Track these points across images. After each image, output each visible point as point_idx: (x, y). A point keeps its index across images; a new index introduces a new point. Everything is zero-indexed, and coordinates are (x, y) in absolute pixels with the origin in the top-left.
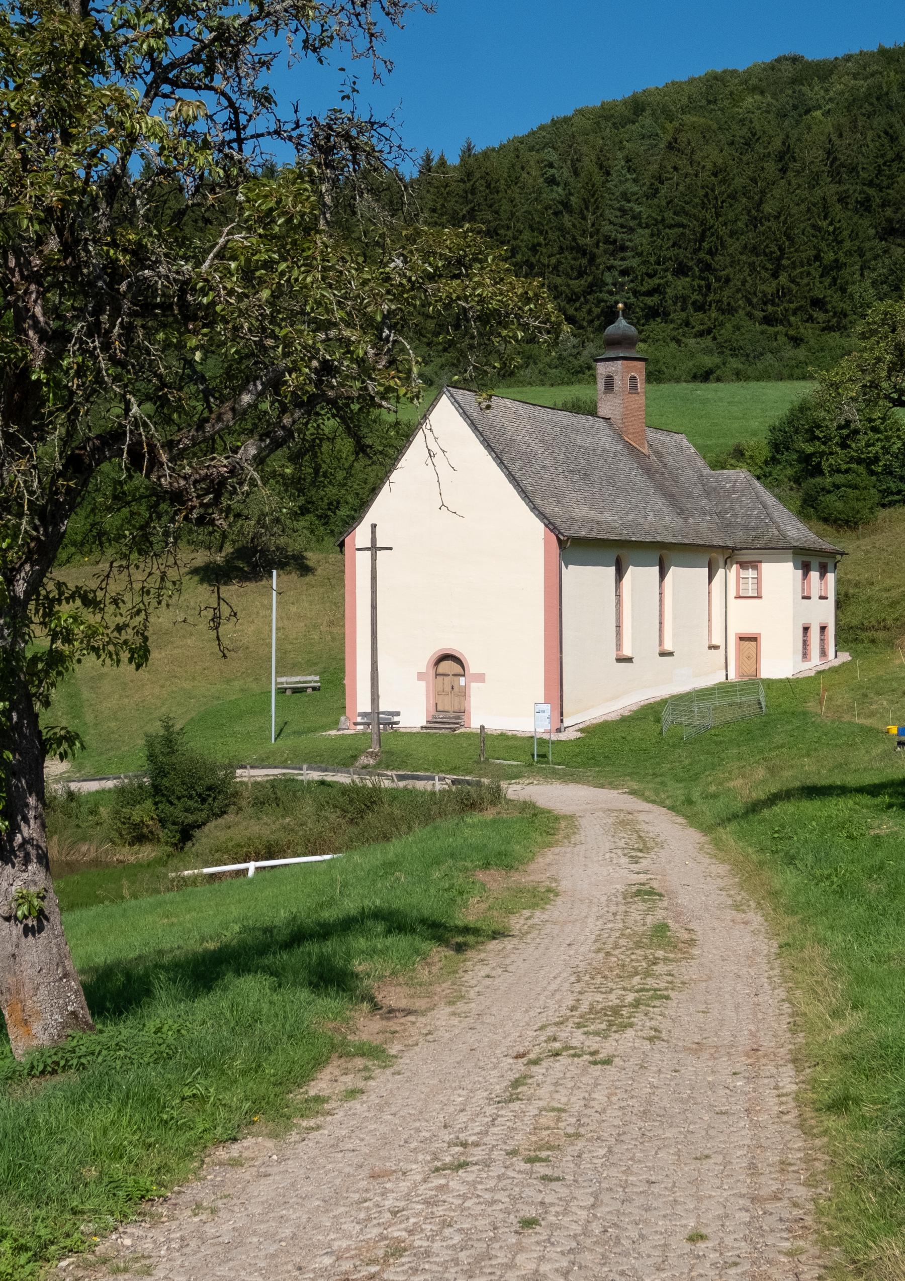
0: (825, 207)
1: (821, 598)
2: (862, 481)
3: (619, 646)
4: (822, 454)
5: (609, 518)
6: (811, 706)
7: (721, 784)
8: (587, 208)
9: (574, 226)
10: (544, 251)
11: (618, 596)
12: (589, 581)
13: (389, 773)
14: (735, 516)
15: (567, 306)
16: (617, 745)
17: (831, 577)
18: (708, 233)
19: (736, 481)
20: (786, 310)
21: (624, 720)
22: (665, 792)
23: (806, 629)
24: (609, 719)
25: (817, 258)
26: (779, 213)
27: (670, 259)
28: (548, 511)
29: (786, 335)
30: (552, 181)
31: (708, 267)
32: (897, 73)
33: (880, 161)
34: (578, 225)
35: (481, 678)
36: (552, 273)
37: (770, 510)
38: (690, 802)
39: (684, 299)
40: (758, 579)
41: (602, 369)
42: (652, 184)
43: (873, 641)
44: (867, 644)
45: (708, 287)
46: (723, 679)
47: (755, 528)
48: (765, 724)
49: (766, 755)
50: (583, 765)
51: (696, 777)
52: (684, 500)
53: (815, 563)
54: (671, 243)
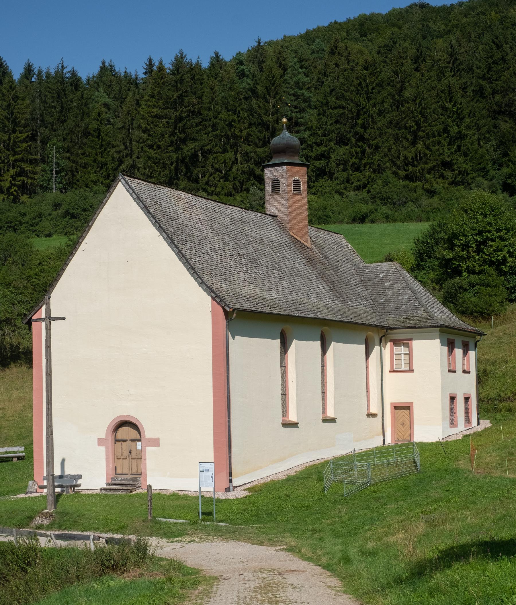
0: (450, 93)
1: (465, 372)
2: (493, 280)
3: (285, 411)
4: (462, 258)
5: (274, 297)
6: (463, 464)
7: (380, 539)
8: (269, 95)
9: (259, 107)
10: (237, 126)
11: (284, 366)
12: (255, 351)
13: (48, 533)
14: (388, 301)
15: (255, 168)
16: (281, 502)
17: (472, 354)
18: (362, 112)
19: (388, 272)
20: (423, 170)
21: (289, 480)
22: (321, 548)
23: (453, 399)
24: (275, 478)
25: (445, 130)
26: (416, 97)
27: (333, 131)
28: (215, 287)
29: (423, 188)
30: (242, 75)
31: (361, 138)
32: (496, 13)
33: (490, 61)
34: (261, 105)
35: (155, 442)
36: (244, 143)
37: (418, 295)
38: (346, 560)
39: (345, 162)
40: (410, 355)
41: (269, 174)
42: (319, 78)
43: (510, 410)
44: (504, 413)
45: (363, 152)
46: (381, 443)
47: (405, 311)
48: (422, 481)
49: (424, 508)
50: (246, 522)
51: (354, 533)
52: (343, 287)
53: (458, 341)
54: (333, 120)
